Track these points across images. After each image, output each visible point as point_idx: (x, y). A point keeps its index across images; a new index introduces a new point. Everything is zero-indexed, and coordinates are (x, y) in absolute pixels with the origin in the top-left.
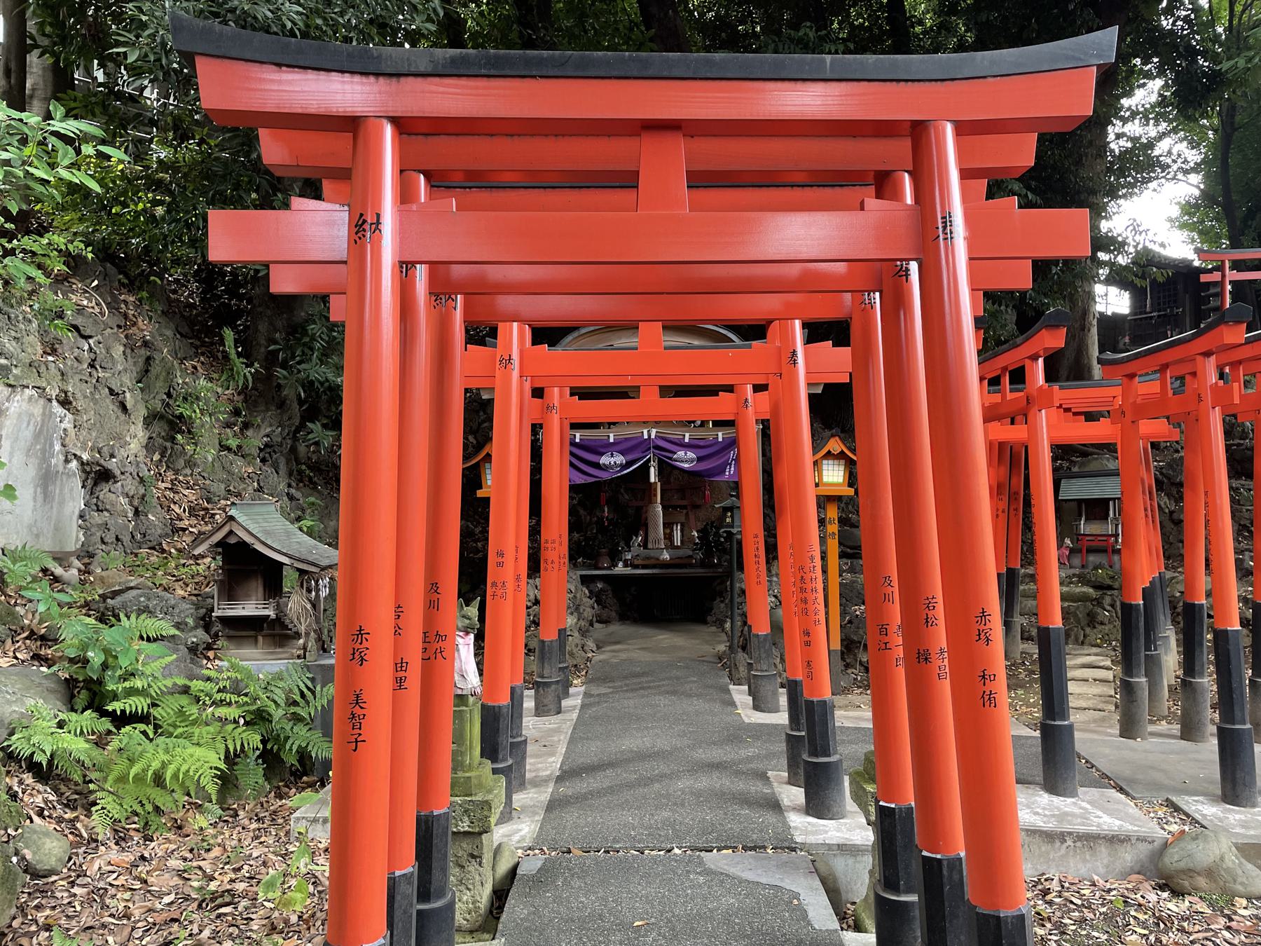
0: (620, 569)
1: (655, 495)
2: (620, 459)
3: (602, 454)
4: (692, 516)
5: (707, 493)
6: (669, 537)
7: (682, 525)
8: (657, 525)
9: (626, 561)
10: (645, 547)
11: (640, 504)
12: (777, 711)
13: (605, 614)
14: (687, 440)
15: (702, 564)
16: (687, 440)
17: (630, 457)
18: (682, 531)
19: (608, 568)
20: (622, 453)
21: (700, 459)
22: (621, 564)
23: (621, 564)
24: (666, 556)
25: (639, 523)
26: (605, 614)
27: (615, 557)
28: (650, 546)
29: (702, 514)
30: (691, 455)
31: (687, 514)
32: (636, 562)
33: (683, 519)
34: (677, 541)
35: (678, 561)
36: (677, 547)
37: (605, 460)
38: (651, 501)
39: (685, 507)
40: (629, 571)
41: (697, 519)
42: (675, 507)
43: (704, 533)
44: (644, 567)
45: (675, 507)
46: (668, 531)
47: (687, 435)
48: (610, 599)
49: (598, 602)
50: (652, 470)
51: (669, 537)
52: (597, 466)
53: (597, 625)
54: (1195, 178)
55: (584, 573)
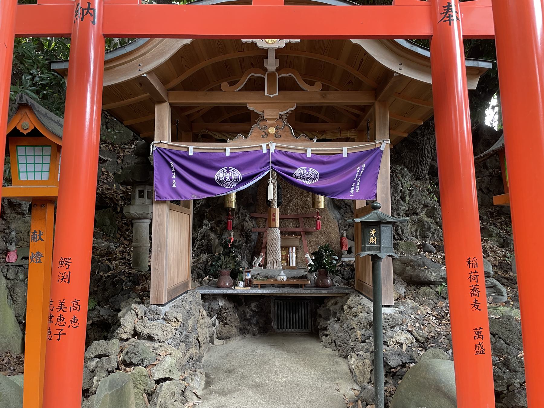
0: (240, 289)
1: (274, 220)
2: (237, 175)
3: (217, 169)
4: (305, 241)
5: (319, 221)
6: (286, 259)
7: (296, 249)
8: (275, 247)
9: (246, 280)
10: (265, 266)
11: (261, 230)
12: (175, 138)
13: (225, 331)
14: (309, 155)
15: (317, 286)
16: (309, 155)
17: (248, 173)
18: (296, 253)
19: (229, 288)
20: (239, 168)
21: (322, 176)
22: (241, 284)
23: (241, 284)
24: (283, 277)
25: (258, 247)
26: (225, 331)
27: (235, 275)
28: (269, 266)
29: (313, 239)
30: (314, 171)
31: (301, 239)
32: (255, 282)
33: (297, 243)
34: (292, 263)
35: (294, 282)
36: (293, 268)
37: (219, 175)
38: (268, 221)
39: (299, 234)
40: (249, 291)
41: (309, 244)
42: (291, 233)
43: (318, 256)
44: (263, 286)
45: (291, 233)
46: (285, 253)
47: (309, 150)
48: (233, 317)
49: (220, 319)
50: (271, 187)
51: (286, 259)
52: (211, 181)
53: (217, 342)
54: (489, 125)
55: (205, 292)
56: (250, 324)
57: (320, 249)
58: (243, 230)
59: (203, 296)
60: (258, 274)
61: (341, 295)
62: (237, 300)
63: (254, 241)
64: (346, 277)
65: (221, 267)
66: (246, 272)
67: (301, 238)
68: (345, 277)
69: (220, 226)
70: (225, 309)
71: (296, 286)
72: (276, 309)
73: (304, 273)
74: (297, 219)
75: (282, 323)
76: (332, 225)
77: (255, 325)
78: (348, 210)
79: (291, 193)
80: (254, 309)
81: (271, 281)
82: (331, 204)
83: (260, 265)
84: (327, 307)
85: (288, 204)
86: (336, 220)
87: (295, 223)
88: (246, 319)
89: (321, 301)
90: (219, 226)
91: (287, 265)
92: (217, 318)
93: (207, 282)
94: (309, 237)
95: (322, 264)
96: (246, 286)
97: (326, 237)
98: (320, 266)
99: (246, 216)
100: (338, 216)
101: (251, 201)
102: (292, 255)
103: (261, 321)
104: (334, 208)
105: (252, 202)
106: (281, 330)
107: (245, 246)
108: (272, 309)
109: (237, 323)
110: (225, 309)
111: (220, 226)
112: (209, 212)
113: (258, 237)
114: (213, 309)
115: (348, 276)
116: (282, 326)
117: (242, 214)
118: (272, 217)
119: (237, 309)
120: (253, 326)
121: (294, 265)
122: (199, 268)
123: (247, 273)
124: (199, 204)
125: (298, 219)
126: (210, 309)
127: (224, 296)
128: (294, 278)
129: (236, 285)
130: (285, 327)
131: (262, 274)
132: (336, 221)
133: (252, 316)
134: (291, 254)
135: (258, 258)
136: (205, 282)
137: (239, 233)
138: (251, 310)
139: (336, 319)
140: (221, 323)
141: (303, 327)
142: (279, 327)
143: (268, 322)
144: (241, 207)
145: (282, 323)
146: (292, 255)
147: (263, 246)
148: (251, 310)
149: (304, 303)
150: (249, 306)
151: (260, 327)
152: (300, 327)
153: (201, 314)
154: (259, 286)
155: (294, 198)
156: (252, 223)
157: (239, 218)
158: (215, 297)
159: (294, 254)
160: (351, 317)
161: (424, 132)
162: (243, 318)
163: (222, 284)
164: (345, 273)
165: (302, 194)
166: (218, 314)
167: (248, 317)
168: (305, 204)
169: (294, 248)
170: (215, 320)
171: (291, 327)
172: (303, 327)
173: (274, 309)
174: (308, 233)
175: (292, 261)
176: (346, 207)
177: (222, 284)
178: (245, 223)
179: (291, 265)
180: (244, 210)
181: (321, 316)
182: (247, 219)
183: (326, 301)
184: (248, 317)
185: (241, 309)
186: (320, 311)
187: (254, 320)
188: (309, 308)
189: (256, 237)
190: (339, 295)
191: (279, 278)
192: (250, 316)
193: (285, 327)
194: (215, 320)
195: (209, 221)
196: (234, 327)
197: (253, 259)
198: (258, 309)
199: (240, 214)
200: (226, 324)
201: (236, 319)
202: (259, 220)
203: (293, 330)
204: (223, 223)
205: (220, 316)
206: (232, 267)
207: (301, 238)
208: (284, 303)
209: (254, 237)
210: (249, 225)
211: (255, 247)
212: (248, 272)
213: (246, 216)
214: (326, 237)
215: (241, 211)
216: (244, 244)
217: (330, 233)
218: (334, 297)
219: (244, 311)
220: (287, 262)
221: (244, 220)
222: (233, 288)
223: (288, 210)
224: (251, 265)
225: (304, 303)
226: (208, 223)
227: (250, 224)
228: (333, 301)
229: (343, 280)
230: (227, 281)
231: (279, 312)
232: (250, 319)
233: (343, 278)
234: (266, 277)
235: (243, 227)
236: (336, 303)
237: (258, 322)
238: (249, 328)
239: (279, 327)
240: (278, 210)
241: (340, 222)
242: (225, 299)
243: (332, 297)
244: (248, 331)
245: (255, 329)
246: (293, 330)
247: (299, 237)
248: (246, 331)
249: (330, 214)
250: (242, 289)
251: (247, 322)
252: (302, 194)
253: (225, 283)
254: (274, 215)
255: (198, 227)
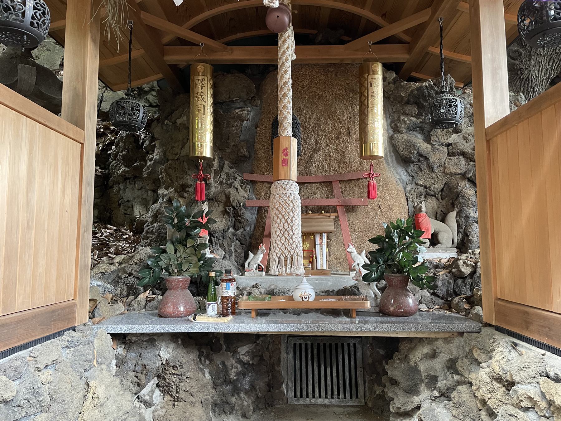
0: (210, 321)
1: (286, 163)
7: (328, 238)
15: (382, 311)
19: (183, 317)
22: (212, 308)
24: (306, 291)
27: (201, 287)
28: (274, 269)
33: (331, 227)
34: (322, 263)
35: (332, 302)
36: (323, 273)
39: (334, 210)
42: (319, 210)
44: (262, 313)
45: (319, 210)
46: (307, 246)
49: (164, 387)
56: (236, 391)
57: (388, 232)
58: (228, 202)
59: (114, 336)
60: (255, 286)
61: (447, 336)
62: (204, 345)
63: (250, 225)
64: (442, 291)
65: (167, 270)
66: (222, 281)
67: (337, 217)
68: (440, 292)
69: (186, 195)
70: (174, 367)
71: (335, 313)
72: (291, 355)
73: (349, 281)
74: (328, 184)
75: (304, 385)
76: (394, 193)
77: (246, 393)
78: (424, 166)
79: (318, 135)
80: (246, 359)
81: (281, 302)
82: (391, 156)
83: (259, 268)
84: (412, 363)
85: (311, 157)
86: (401, 185)
87: (325, 191)
88: (228, 382)
89: (391, 347)
90: (183, 197)
91: (312, 269)
92: (158, 385)
93: (143, 303)
94: (352, 217)
95: (390, 261)
96: (224, 313)
97: (382, 216)
98: (390, 266)
99: (235, 179)
100: (405, 177)
101: (244, 151)
102: (321, 249)
103: (261, 384)
104: (398, 163)
105: (246, 153)
106: (301, 402)
107: (233, 234)
108: (284, 355)
109: (209, 394)
110: (174, 367)
111: (186, 195)
112: (166, 171)
113: (257, 218)
114: (145, 366)
115: (444, 289)
116: (304, 393)
117: (228, 175)
118: (282, 157)
119: (210, 360)
120: (242, 395)
121: (325, 267)
122: (130, 274)
123: (224, 284)
124: (151, 160)
125: (330, 182)
126: (139, 368)
127: (175, 337)
128: (328, 293)
129: (202, 309)
130: (311, 395)
131: (263, 285)
132: (400, 187)
133: (242, 374)
134: (318, 247)
135: (255, 254)
136: (139, 304)
137: (221, 209)
138: (240, 361)
139: (436, 393)
140: (167, 397)
141: (348, 396)
142: (298, 394)
143: (273, 385)
144: (226, 162)
145: (304, 385)
146: (321, 249)
147: (266, 232)
148: (240, 361)
149: (349, 345)
150: (235, 352)
151: (258, 397)
152: (342, 395)
153: (90, 395)
154: (253, 314)
155: (324, 145)
156: (246, 191)
157: (221, 183)
158: (152, 339)
159: (324, 247)
160: (513, 410)
161: (530, 52)
162: (221, 379)
163: (170, 308)
164: (439, 283)
165: (337, 138)
166: (159, 376)
167: (233, 376)
168: (344, 156)
169: (324, 236)
170: (153, 392)
171: (323, 394)
172: (348, 396)
173: (287, 357)
174: (350, 209)
175: (322, 259)
176: (419, 161)
177: (170, 308)
178: (232, 190)
179: (319, 267)
180: (231, 168)
181: (394, 383)
182: (237, 184)
183: (403, 347)
184: (233, 376)
185: (218, 360)
186: (395, 370)
187: (246, 383)
188: (359, 355)
189: (254, 217)
190: (442, 335)
191: (297, 295)
192: (237, 374)
193: (311, 395)
194: (153, 392)
195: (167, 188)
196: (198, 405)
197: (246, 257)
198: (253, 359)
199: (224, 176)
200: (178, 400)
201: (205, 385)
202: (259, 185)
203: (326, 401)
204: (191, 189)
205: (162, 383)
206: (194, 271)
207: (337, 217)
208: (306, 344)
209: (250, 216)
210: (240, 195)
211: (252, 236)
212: (227, 281)
213: (235, 179)
214: (382, 216)
215: (226, 169)
216: (231, 230)
217: (390, 209)
218: (430, 341)
219: (223, 363)
220: (312, 262)
221: (230, 185)
222: (191, 318)
223: (313, 168)
224: (242, 269)
225: (349, 345)
226: (166, 192)
227: (242, 192)
228: (426, 349)
229: (435, 299)
230: (181, 300)
231: (298, 362)
232: (237, 380)
233: (433, 294)
234: (271, 293)
235: (228, 197)
236: (433, 355)
237: (253, 387)
238: (233, 400)
239: (298, 394)
240: (294, 141)
241: (409, 188)
242: (175, 342)
243: (421, 339)
244: (233, 408)
245: (247, 402)
246: (326, 401)
247: (333, 216)
248: (227, 409)
249: (389, 174)
250: (211, 320)
251: (229, 388)
252: (337, 138)
253: (175, 306)
254: (286, 152)
255: (151, 202)
